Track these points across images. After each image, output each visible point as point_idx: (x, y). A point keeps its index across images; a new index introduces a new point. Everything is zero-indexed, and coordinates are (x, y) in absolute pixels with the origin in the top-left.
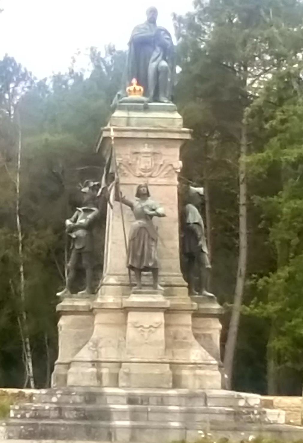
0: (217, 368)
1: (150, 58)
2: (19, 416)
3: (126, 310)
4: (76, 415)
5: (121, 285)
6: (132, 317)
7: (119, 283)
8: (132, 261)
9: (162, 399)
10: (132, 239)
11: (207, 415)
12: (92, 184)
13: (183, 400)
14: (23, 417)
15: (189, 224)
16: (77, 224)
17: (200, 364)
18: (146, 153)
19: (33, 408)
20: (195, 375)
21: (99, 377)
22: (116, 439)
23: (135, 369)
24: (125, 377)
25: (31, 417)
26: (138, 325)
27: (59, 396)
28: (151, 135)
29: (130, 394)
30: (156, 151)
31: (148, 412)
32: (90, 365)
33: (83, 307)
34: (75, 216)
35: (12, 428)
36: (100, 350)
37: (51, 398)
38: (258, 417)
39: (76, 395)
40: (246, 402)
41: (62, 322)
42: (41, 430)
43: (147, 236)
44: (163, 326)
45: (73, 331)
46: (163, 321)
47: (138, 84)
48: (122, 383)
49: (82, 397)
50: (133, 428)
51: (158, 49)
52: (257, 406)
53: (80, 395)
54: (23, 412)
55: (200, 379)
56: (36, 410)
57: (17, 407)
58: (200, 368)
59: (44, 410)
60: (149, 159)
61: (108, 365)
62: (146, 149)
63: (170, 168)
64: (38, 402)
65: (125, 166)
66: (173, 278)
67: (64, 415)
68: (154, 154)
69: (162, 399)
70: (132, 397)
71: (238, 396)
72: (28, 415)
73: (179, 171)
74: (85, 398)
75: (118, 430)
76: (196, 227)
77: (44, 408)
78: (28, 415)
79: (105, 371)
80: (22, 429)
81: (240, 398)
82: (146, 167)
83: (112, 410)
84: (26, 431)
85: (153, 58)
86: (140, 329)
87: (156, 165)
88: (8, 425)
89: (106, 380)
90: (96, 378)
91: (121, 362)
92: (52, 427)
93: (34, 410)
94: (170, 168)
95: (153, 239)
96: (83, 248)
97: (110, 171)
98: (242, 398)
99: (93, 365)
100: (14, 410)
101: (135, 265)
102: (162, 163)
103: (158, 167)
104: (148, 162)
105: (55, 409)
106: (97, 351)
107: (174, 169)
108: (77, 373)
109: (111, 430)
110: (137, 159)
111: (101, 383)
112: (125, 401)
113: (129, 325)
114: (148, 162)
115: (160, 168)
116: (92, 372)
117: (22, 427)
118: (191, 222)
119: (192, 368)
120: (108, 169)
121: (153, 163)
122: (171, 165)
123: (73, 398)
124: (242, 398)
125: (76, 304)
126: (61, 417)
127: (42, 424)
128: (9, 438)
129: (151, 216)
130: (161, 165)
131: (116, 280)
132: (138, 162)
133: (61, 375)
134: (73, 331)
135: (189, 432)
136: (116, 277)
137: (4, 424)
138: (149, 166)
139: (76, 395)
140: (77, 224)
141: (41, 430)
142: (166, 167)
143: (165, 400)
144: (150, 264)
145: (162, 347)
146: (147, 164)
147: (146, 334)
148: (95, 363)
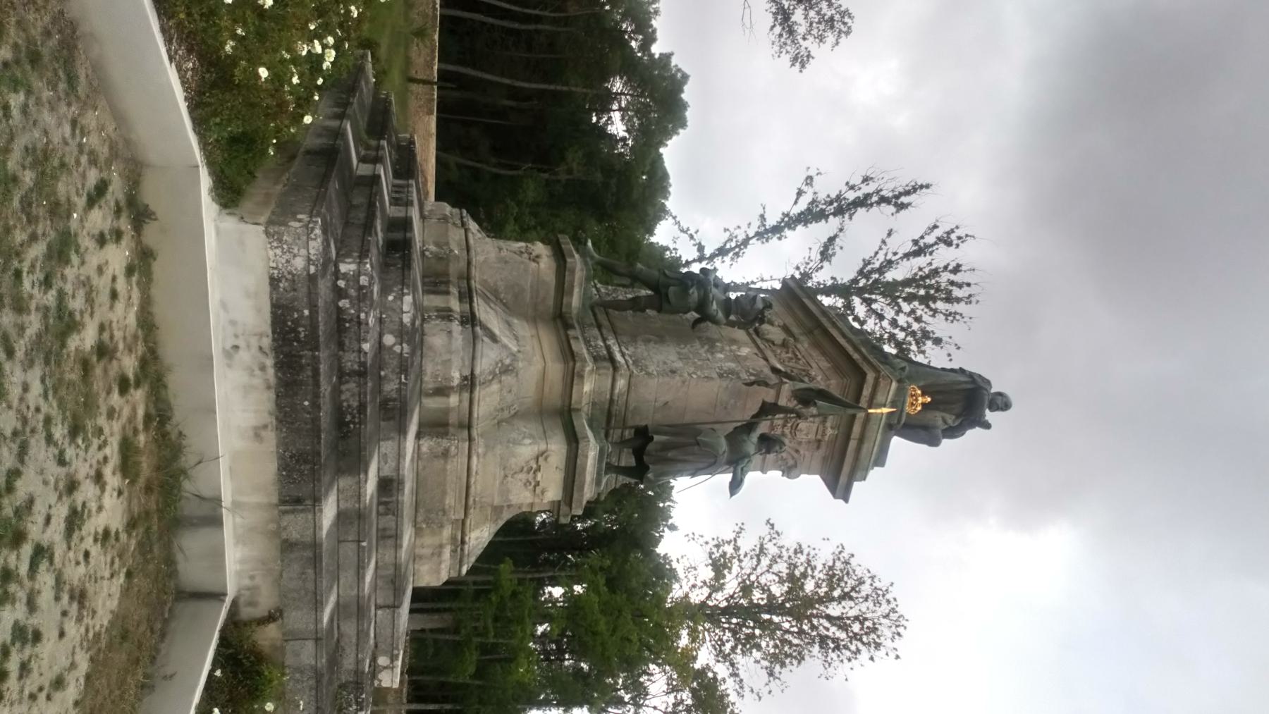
0: (454, 574)
1: (944, 411)
2: (341, 283)
4: (349, 406)
5: (611, 401)
6: (557, 448)
9: (390, 537)
11: (354, 640)
13: (391, 571)
14: (340, 293)
17: (462, 550)
18: (824, 434)
19: (363, 316)
20: (441, 546)
21: (442, 391)
22: (286, 512)
23: (456, 465)
24: (440, 449)
25: (340, 311)
27: (397, 349)
28: (853, 444)
29: (401, 483)
30: (823, 445)
31: (359, 541)
32: (467, 373)
33: (570, 304)
35: (303, 291)
36: (496, 381)
37: (391, 333)
39: (400, 383)
40: (385, 668)
42: (301, 357)
45: (527, 283)
47: (923, 404)
48: (426, 445)
49: (394, 395)
50: (315, 545)
52: (376, 683)
53: (399, 390)
54: (352, 292)
55: (433, 554)
57: (364, 280)
58: (454, 551)
59: (360, 340)
61: (466, 404)
67: (347, 382)
69: (390, 537)
70: (395, 485)
71: (397, 656)
72: (344, 303)
74: (390, 400)
75: (310, 516)
77: (366, 341)
78: (344, 303)
79: (453, 400)
80: (300, 312)
81: (393, 658)
83: (362, 476)
84: (296, 322)
86: (535, 466)
87: (800, 443)
88: (312, 279)
89: (433, 403)
90: (437, 385)
91: (469, 427)
92: (311, 381)
93: (358, 317)
96: (669, 302)
98: (392, 661)
99: (465, 378)
100: (358, 274)
103: (796, 446)
104: (807, 435)
105: (363, 364)
106: (495, 375)
108: (450, 352)
109: (308, 502)
111: (428, 395)
112: (388, 471)
114: (807, 435)
116: (451, 379)
117: (306, 312)
119: (453, 538)
124: (392, 661)
125: (576, 290)
126: (342, 375)
127: (316, 360)
128: (274, 282)
130: (797, 451)
133: (447, 265)
134: (527, 283)
135: (310, 645)
137: (312, 269)
139: (400, 383)
141: (301, 357)
143: (390, 542)
145: (497, 501)
147: (523, 476)
148: (470, 382)
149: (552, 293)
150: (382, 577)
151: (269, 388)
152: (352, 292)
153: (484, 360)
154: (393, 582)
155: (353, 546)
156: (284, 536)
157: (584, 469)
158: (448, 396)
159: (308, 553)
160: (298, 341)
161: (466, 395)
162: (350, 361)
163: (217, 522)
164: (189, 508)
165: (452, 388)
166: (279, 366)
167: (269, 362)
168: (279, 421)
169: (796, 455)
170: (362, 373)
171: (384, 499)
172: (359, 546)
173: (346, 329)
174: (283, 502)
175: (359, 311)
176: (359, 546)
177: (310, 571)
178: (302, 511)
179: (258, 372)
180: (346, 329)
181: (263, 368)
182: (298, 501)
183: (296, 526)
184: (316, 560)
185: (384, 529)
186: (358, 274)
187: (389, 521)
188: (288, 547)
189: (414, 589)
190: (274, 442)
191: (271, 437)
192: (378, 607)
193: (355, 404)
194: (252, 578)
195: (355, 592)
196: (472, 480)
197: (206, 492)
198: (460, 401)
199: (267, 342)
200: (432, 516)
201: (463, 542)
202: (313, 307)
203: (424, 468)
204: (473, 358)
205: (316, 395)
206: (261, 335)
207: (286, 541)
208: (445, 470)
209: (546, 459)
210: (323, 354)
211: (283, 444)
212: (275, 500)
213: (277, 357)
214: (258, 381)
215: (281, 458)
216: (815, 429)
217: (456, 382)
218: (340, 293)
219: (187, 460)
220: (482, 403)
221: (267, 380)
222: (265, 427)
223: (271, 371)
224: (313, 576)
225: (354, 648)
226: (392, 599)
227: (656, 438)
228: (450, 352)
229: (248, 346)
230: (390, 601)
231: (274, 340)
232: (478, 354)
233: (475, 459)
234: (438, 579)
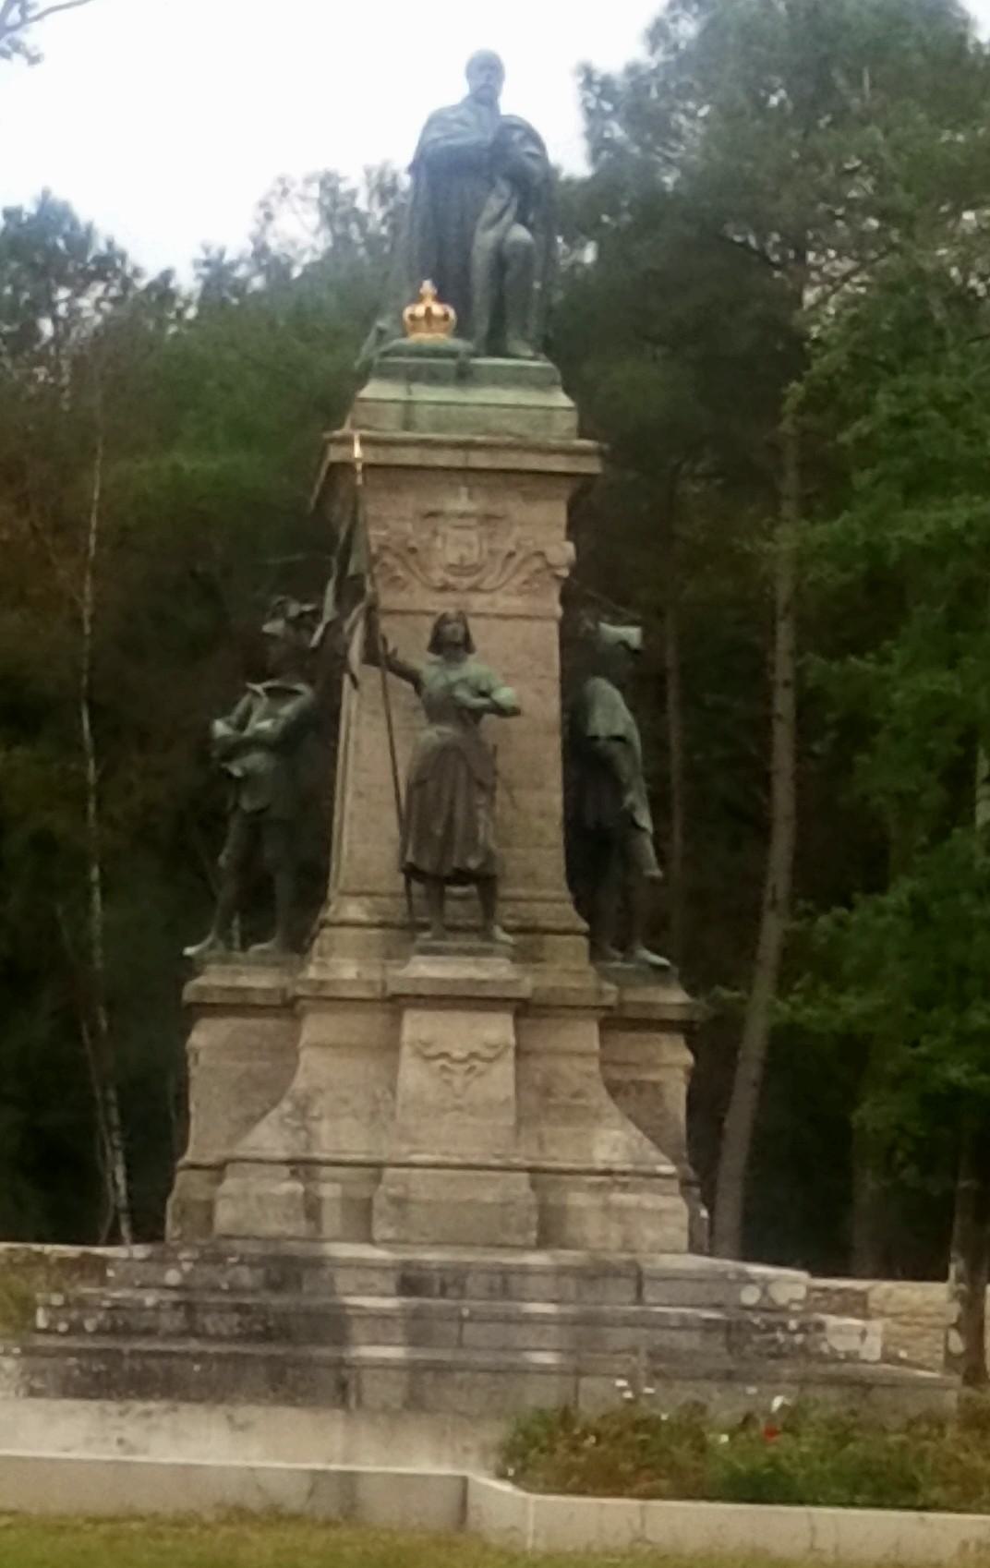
2: (63, 1327)
3: (396, 1003)
4: (240, 1325)
6: (416, 1026)
7: (377, 919)
8: (418, 850)
9: (505, 1282)
10: (417, 784)
11: (645, 1331)
12: (294, 609)
15: (596, 738)
16: (247, 733)
17: (624, 1173)
19: (106, 1304)
20: (607, 1208)
21: (312, 1209)
22: (359, 1401)
23: (423, 1186)
24: (392, 1210)
25: (100, 1331)
26: (432, 1051)
27: (187, 1267)
28: (479, 460)
30: (497, 508)
33: (267, 992)
34: (240, 709)
37: (163, 1275)
38: (799, 1338)
40: (765, 1292)
41: (203, 1037)
42: (132, 1370)
43: (463, 774)
44: (511, 1054)
46: (512, 1040)
49: (260, 1272)
51: (504, 187)
52: (795, 1307)
53: (252, 1265)
55: (622, 1221)
56: (116, 1307)
57: (57, 1300)
59: (141, 1308)
60: (473, 536)
62: (460, 502)
63: (537, 563)
64: (121, 1284)
65: (397, 555)
66: (539, 907)
67: (204, 1326)
68: (488, 518)
69: (505, 1282)
70: (412, 1273)
72: (89, 1325)
73: (565, 573)
75: (367, 1374)
76: (615, 747)
78: (89, 1325)
79: (329, 1191)
80: (70, 1368)
81: (750, 1280)
82: (462, 558)
83: (350, 1312)
85: (487, 215)
86: (442, 1062)
87: (492, 553)
89: (332, 1219)
91: (379, 1166)
92: (165, 1361)
94: (537, 563)
95: (481, 785)
97: (352, 570)
99: (294, 1174)
100: (48, 1306)
101: (426, 865)
102: (511, 546)
107: (549, 566)
109: (345, 1373)
110: (435, 533)
111: (319, 1229)
113: (406, 1050)
114: (470, 545)
115: (504, 567)
118: (602, 733)
120: (344, 565)
121: (485, 546)
122: (541, 554)
123: (231, 1273)
125: (243, 981)
127: (133, 1354)
128: (33, 1393)
129: (477, 714)
130: (511, 555)
131: (369, 912)
132: (438, 543)
135: (584, 1382)
136: (366, 901)
138: (473, 556)
139: (241, 1263)
140: (247, 733)
141: (132, 1370)
142: (524, 561)
143: (514, 1280)
144: (473, 863)
146: (465, 551)
148: (302, 1167)
149: (253, 1023)
150: (579, 1293)
151: (175, 1410)
152: (74, 1315)
153: (267, 1144)
154: (593, 1278)
155: (469, 1329)
156: (397, 1406)
157: (442, 981)
158: (320, 1200)
159: (428, 1377)
160: (108, 1373)
161: (325, 1171)
162: (172, 1321)
163: (349, 1479)
164: (327, 1506)
165: (306, 1194)
166: (144, 1395)
167: (139, 1406)
168: (221, 1400)
169: (520, 556)
170: (190, 1308)
171: (437, 1288)
172: (470, 1319)
173: (126, 1324)
174: (343, 1403)
175: (100, 1308)
176: (470, 1319)
177: (459, 1376)
178: (359, 1382)
179: (154, 1420)
180: (126, 1324)
181: (148, 1414)
182: (343, 1386)
183: (378, 1390)
184: (440, 1369)
185: (491, 1289)
186: (48, 1306)
187: (475, 1284)
188: (415, 1403)
189: (694, 1248)
190: (251, 1407)
191: (245, 1412)
192: (639, 1300)
193: (236, 1318)
194: (466, 1450)
195: (553, 1328)
196: (456, 1160)
197: (306, 1486)
198: (334, 1180)
199: (113, 1407)
200: (513, 1220)
201: (608, 1173)
202: (70, 1352)
203: (424, 1234)
204: (260, 1161)
205: (185, 1355)
206: (103, 1411)
207: (406, 1405)
208: (428, 1203)
209: (428, 1045)
210: (126, 1347)
211: (255, 1398)
212: (339, 1413)
213: (132, 1398)
214: (166, 1421)
215: (276, 1402)
216: (457, 533)
217: (299, 1187)
218: (76, 1329)
219: (254, 1502)
220: (345, 1146)
221: (166, 1412)
222: (230, 1418)
223: (152, 1405)
224: (467, 1375)
225: (658, 1332)
226: (622, 1281)
227: (410, 857)
228: (245, 1196)
229: (120, 1428)
230: (630, 1285)
231: (110, 1398)
232: (258, 1154)
233: (416, 1158)
234: (675, 1212)
